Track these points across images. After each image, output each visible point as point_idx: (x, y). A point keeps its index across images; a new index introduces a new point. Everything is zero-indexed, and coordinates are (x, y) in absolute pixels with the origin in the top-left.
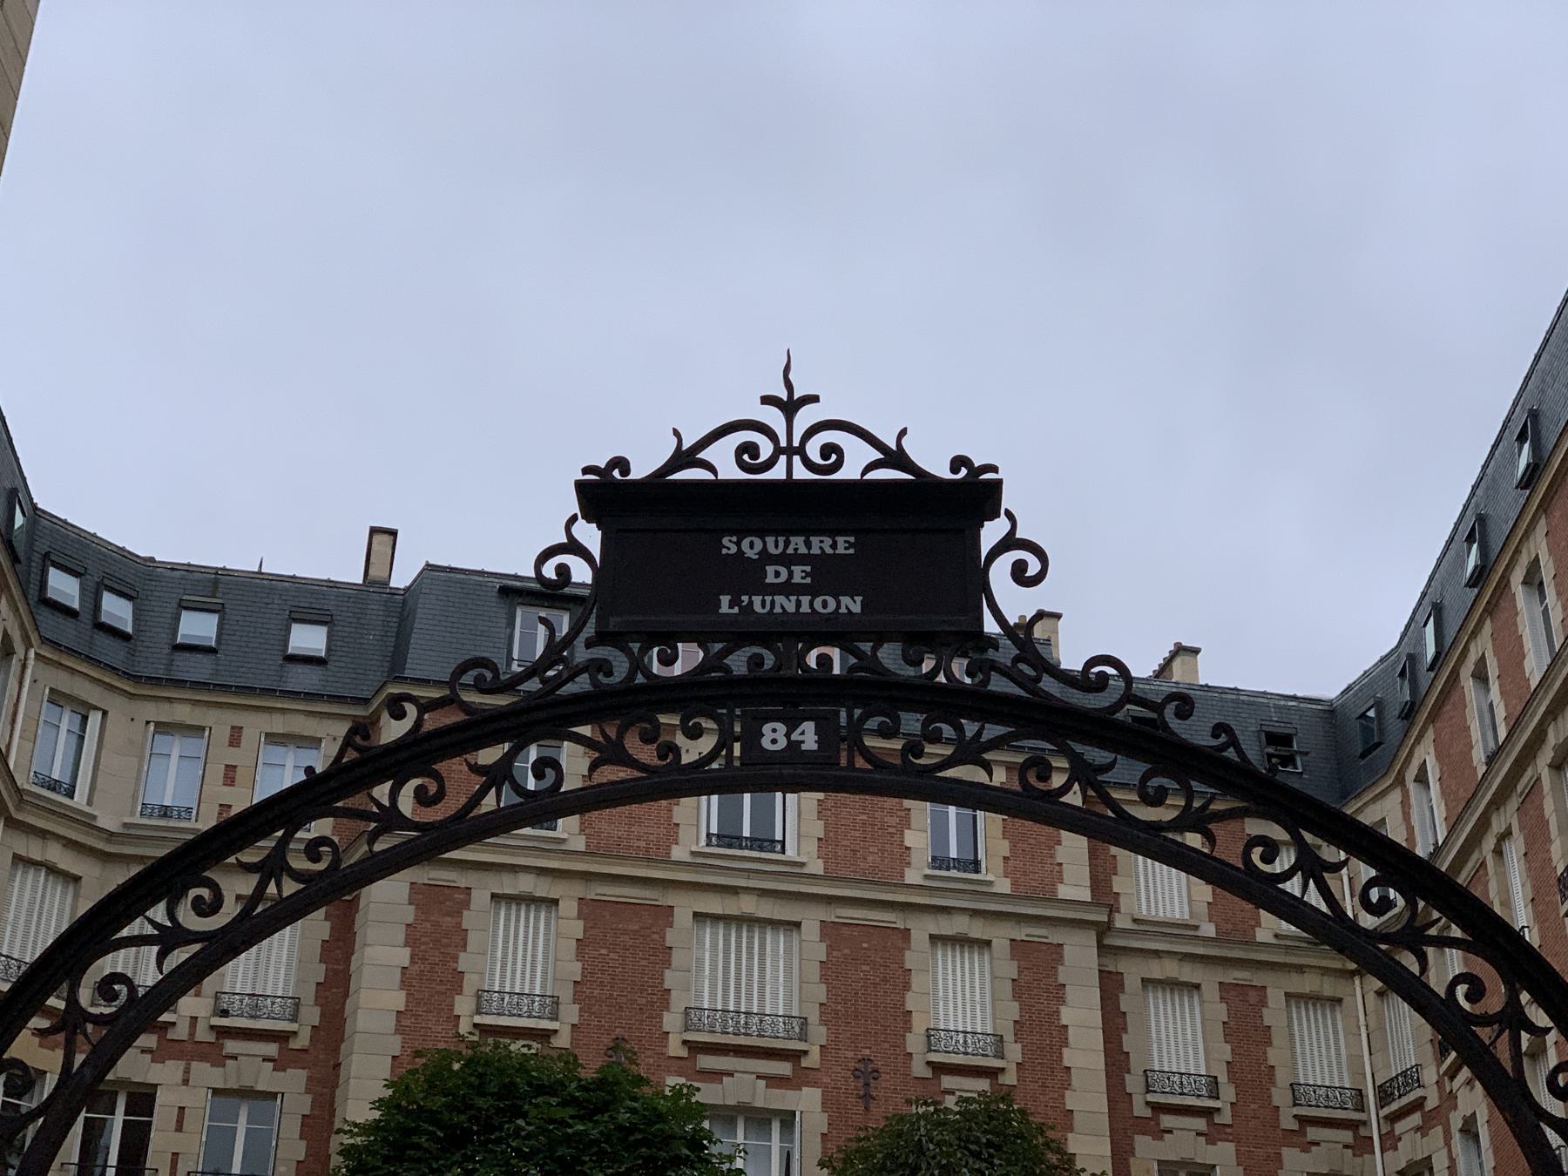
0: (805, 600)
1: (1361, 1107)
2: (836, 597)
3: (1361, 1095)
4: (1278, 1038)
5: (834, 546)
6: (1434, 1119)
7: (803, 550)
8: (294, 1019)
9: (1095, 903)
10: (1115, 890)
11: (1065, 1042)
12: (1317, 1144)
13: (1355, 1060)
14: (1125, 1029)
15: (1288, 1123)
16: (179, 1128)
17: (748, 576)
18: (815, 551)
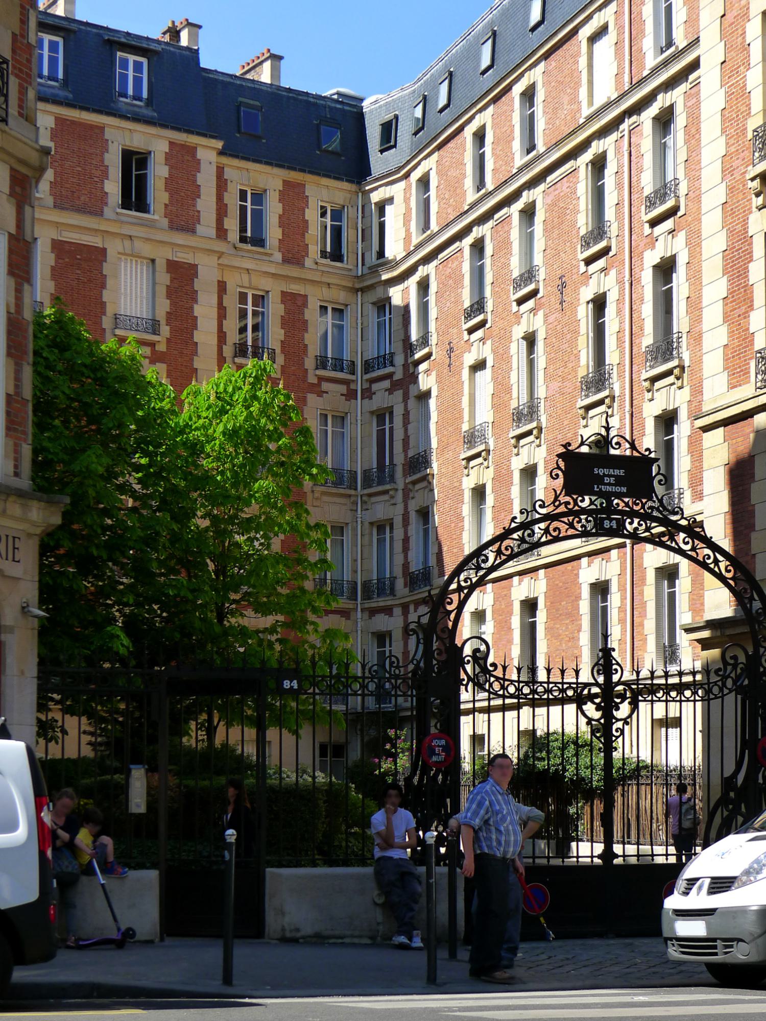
3: (354, 365)
10: (225, 227)
11: (195, 327)
12: (327, 392)
15: (312, 380)
17: (600, 480)
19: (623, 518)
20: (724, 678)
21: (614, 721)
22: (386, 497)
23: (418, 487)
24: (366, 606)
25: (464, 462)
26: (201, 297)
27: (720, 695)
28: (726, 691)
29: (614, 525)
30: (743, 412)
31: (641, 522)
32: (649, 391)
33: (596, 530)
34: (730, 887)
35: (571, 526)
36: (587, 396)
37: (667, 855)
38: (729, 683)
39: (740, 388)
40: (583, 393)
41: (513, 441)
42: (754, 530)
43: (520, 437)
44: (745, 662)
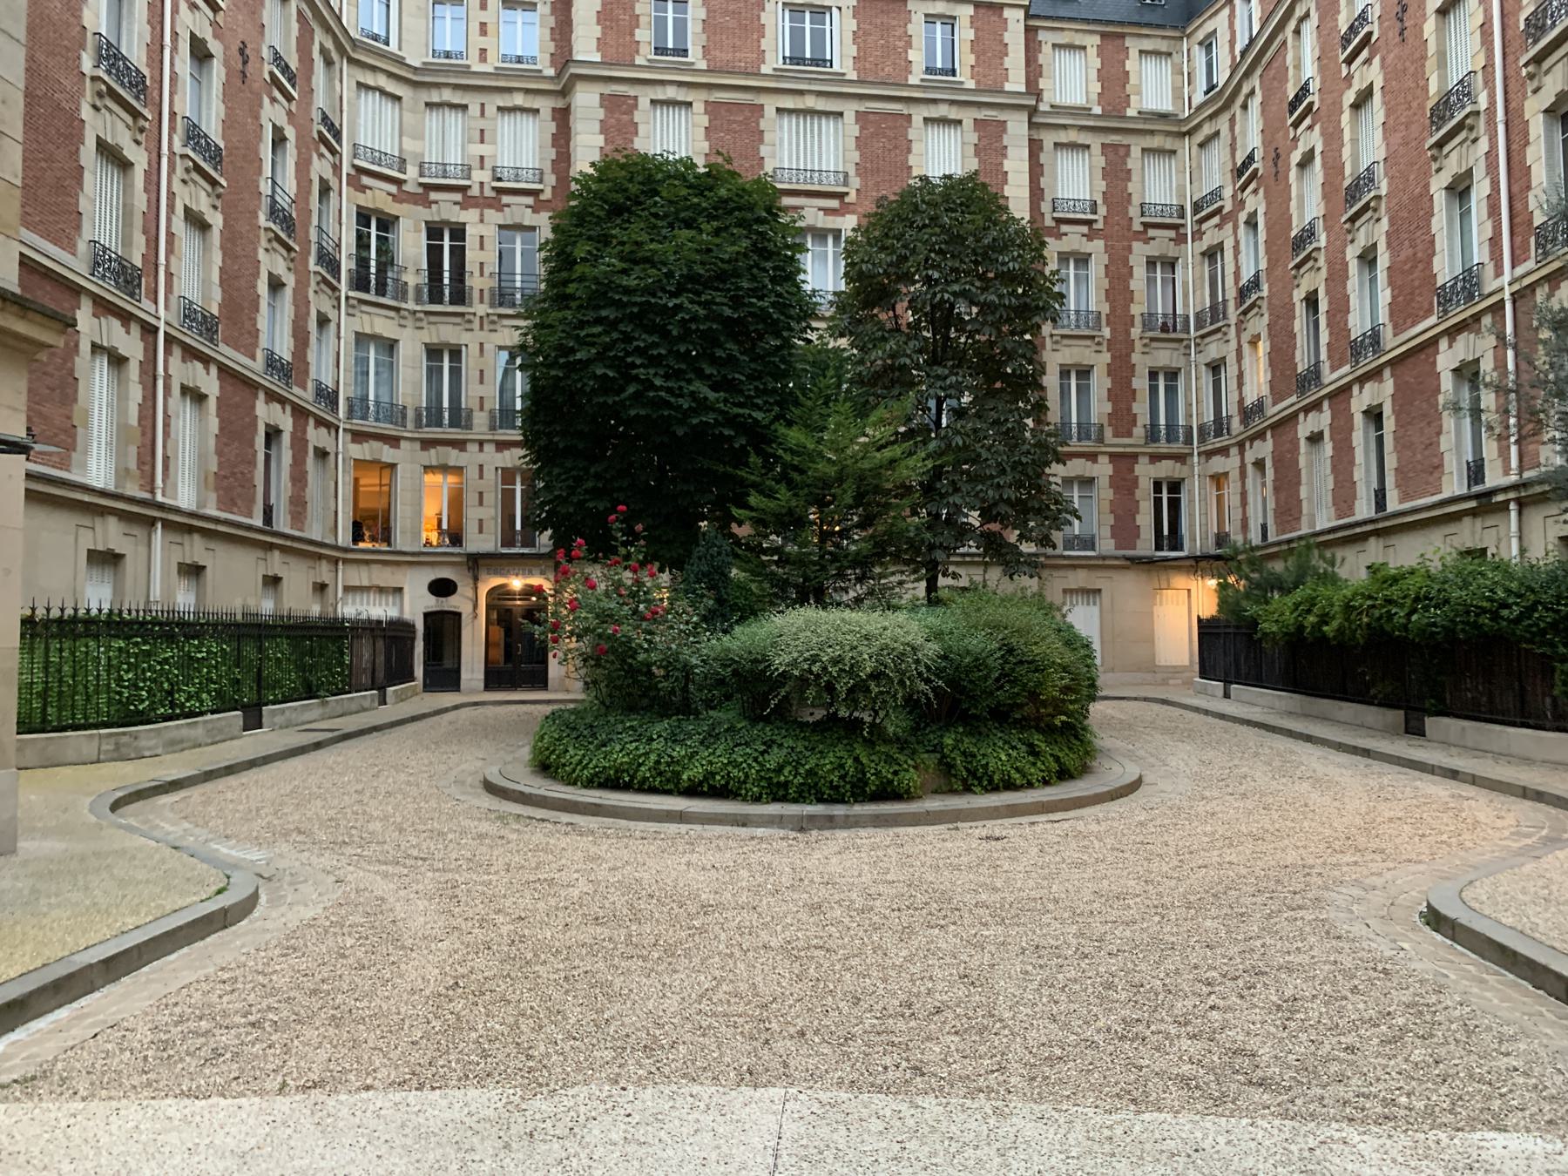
1: (1182, 216)
4: (1135, 177)
6: (1226, 218)
8: (541, 182)
9: (1028, 93)
13: (1181, 188)
14: (1042, 175)
16: (482, 248)
22: (1219, 335)
24: (1202, 449)
26: (1010, 152)
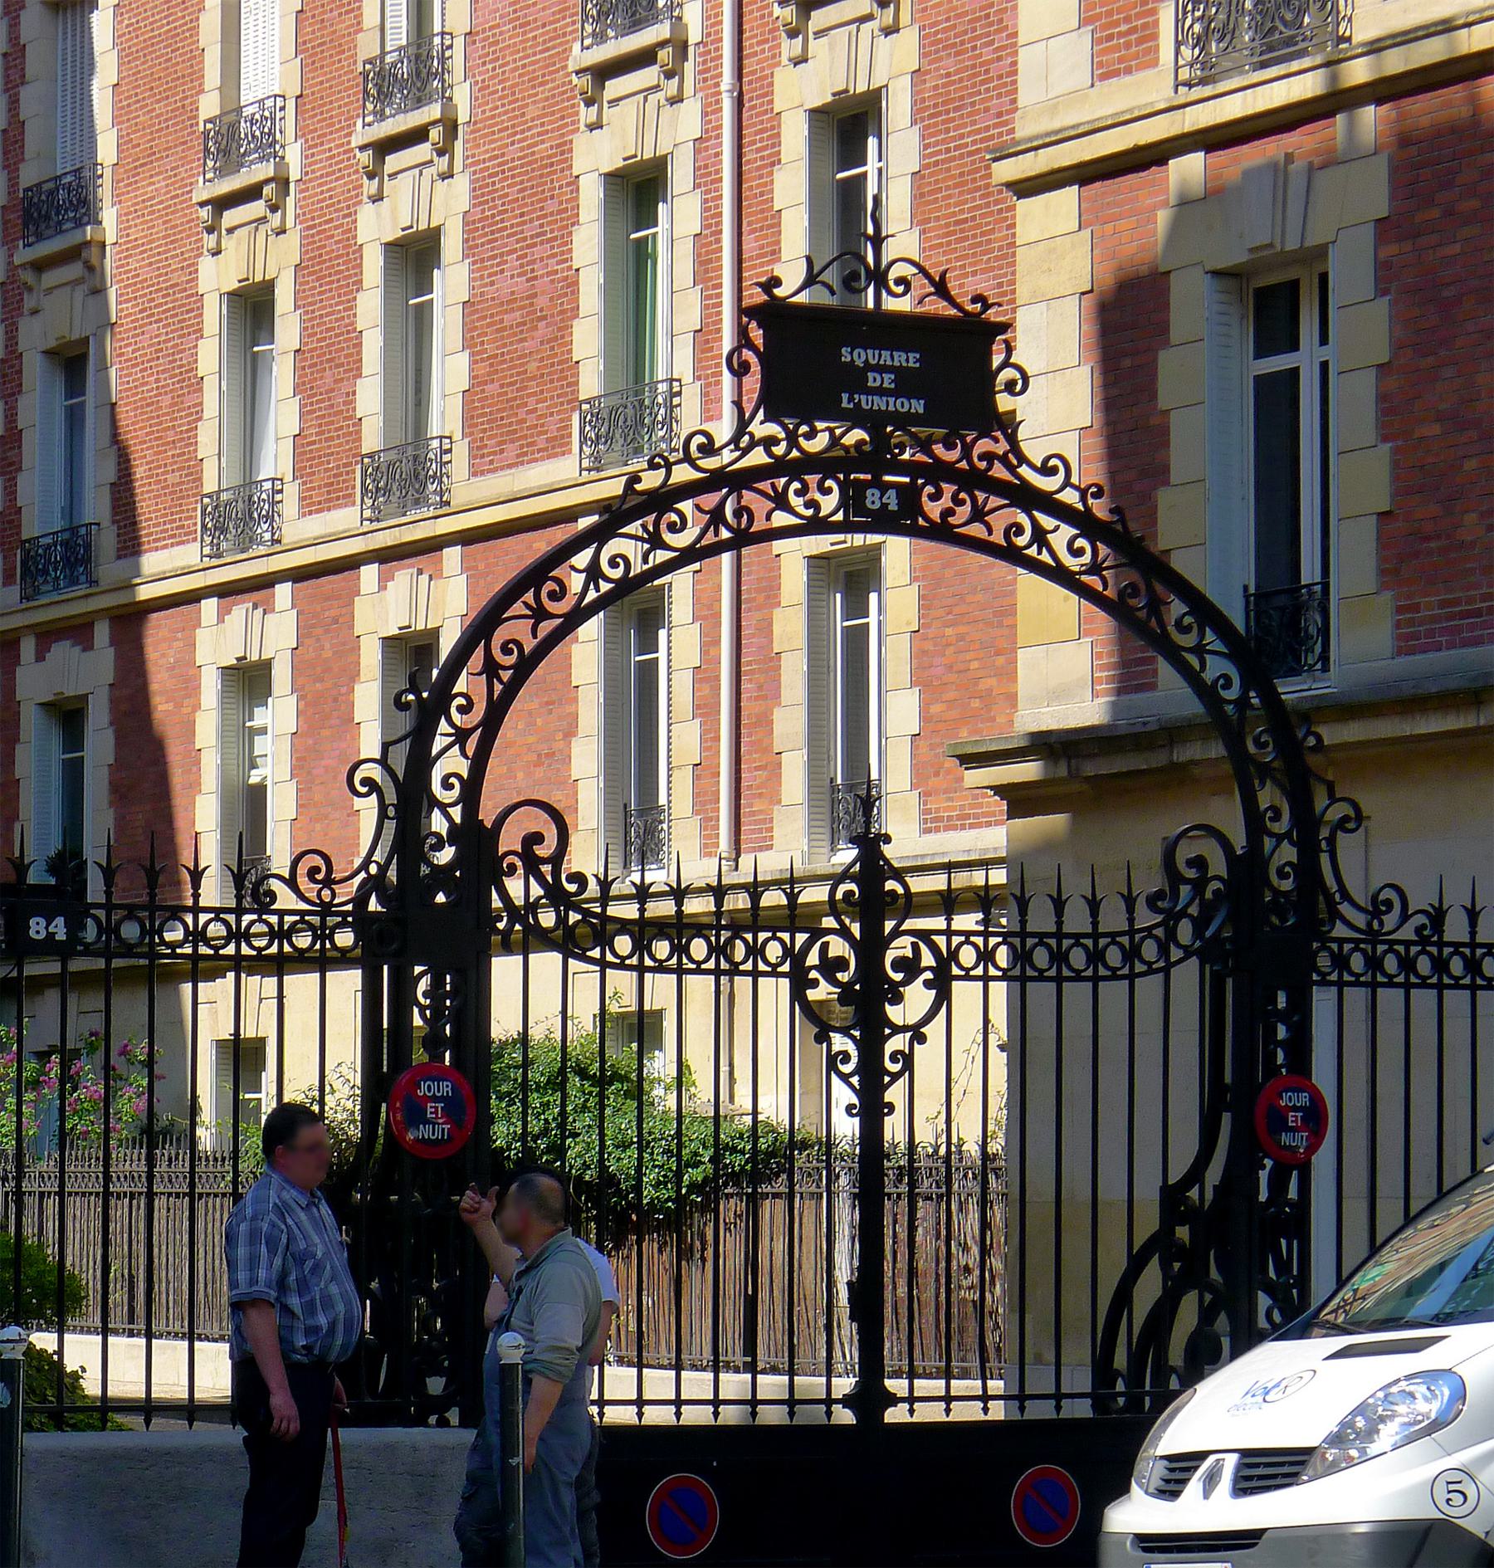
0: (891, 400)
2: (909, 400)
5: (907, 360)
7: (889, 363)
17: (855, 380)
18: (896, 364)
19: (914, 481)
20: (1172, 918)
21: (887, 1031)
23: (51, 278)
25: (205, 213)
27: (1162, 964)
28: (1176, 954)
29: (892, 500)
30: (1137, 150)
31: (962, 495)
32: (792, 34)
33: (846, 514)
34: (1296, 1475)
35: (781, 502)
36: (600, 38)
37: (985, 1398)
38: (1185, 932)
39: (1128, 79)
40: (589, 29)
41: (365, 158)
42: (1167, 483)
43: (386, 147)
44: (1225, 875)
